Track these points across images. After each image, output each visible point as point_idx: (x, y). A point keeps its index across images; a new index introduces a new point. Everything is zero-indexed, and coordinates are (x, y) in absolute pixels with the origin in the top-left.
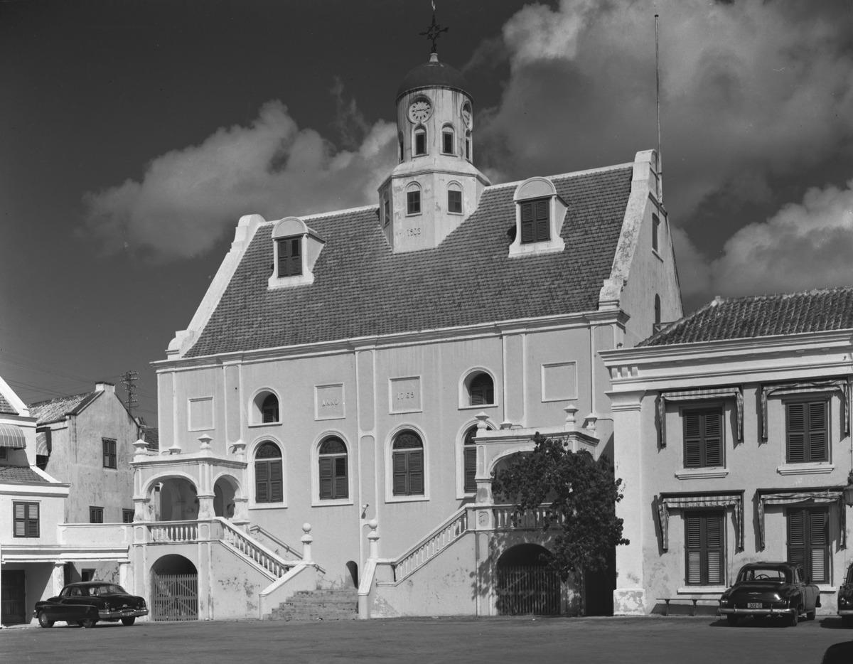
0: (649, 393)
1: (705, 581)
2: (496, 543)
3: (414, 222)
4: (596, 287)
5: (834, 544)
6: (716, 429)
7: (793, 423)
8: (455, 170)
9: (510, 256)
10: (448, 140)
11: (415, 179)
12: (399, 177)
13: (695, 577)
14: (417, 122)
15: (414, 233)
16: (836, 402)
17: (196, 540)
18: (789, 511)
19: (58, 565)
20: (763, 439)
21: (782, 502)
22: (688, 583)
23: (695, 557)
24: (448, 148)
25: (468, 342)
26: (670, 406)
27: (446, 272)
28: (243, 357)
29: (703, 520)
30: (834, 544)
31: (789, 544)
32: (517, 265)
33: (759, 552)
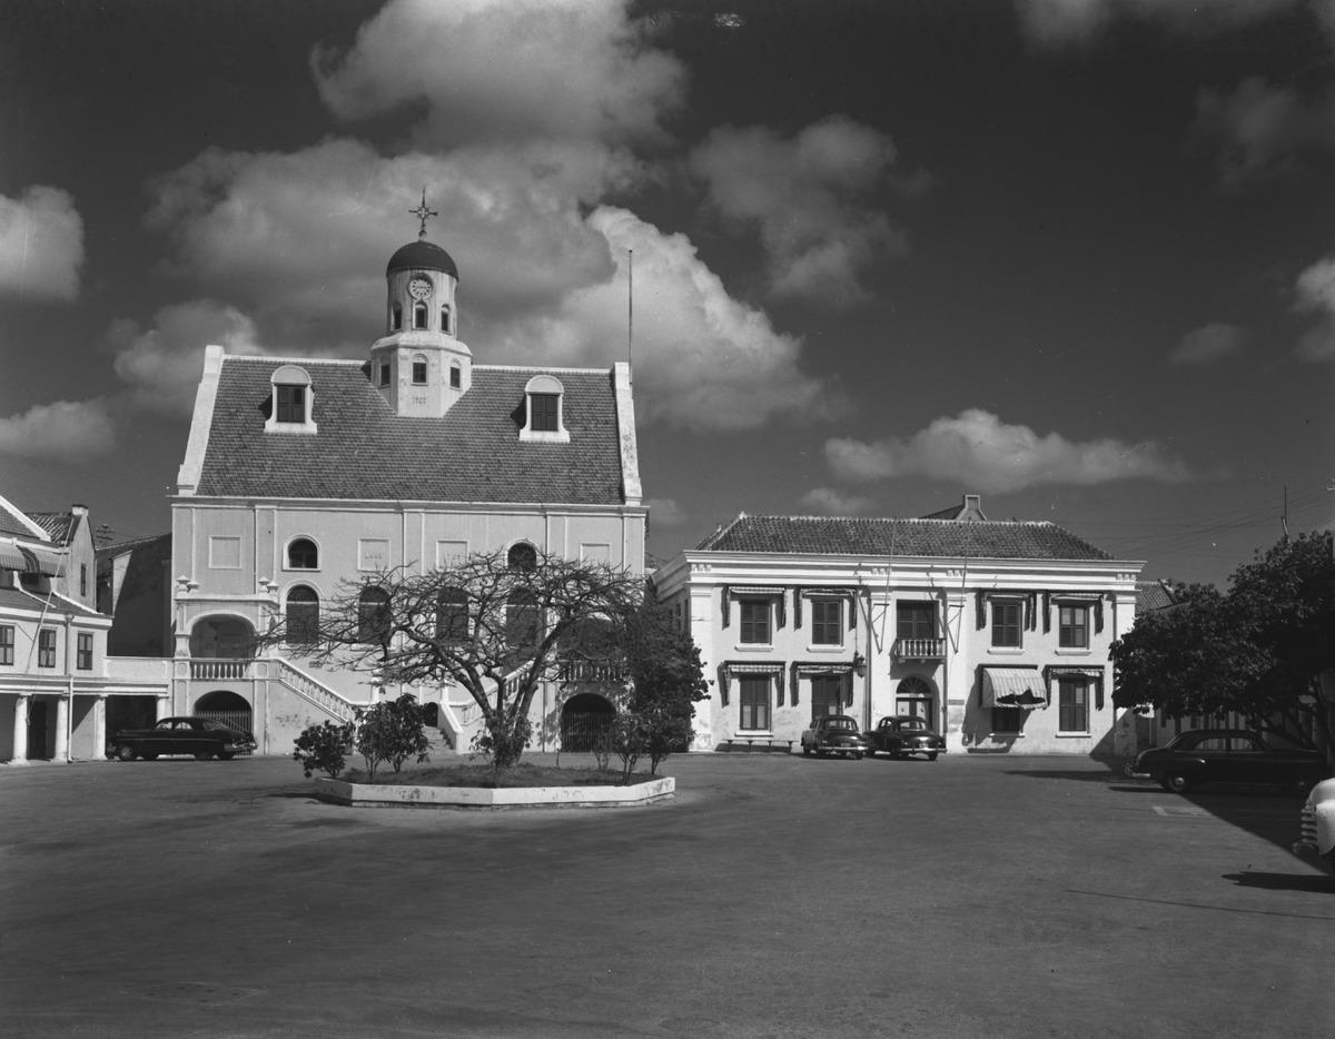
0: (718, 585)
1: (754, 727)
2: (561, 698)
3: (419, 391)
5: (844, 704)
6: (765, 616)
7: (817, 616)
8: (455, 349)
10: (445, 317)
11: (422, 352)
12: (406, 347)
13: (747, 723)
14: (419, 298)
15: (420, 401)
16: (846, 603)
18: (814, 678)
19: (102, 699)
20: (798, 624)
21: (812, 672)
22: (742, 728)
23: (747, 709)
24: (445, 327)
25: (515, 517)
26: (735, 596)
27: (461, 444)
28: (280, 503)
29: (754, 683)
30: (844, 704)
31: (813, 701)
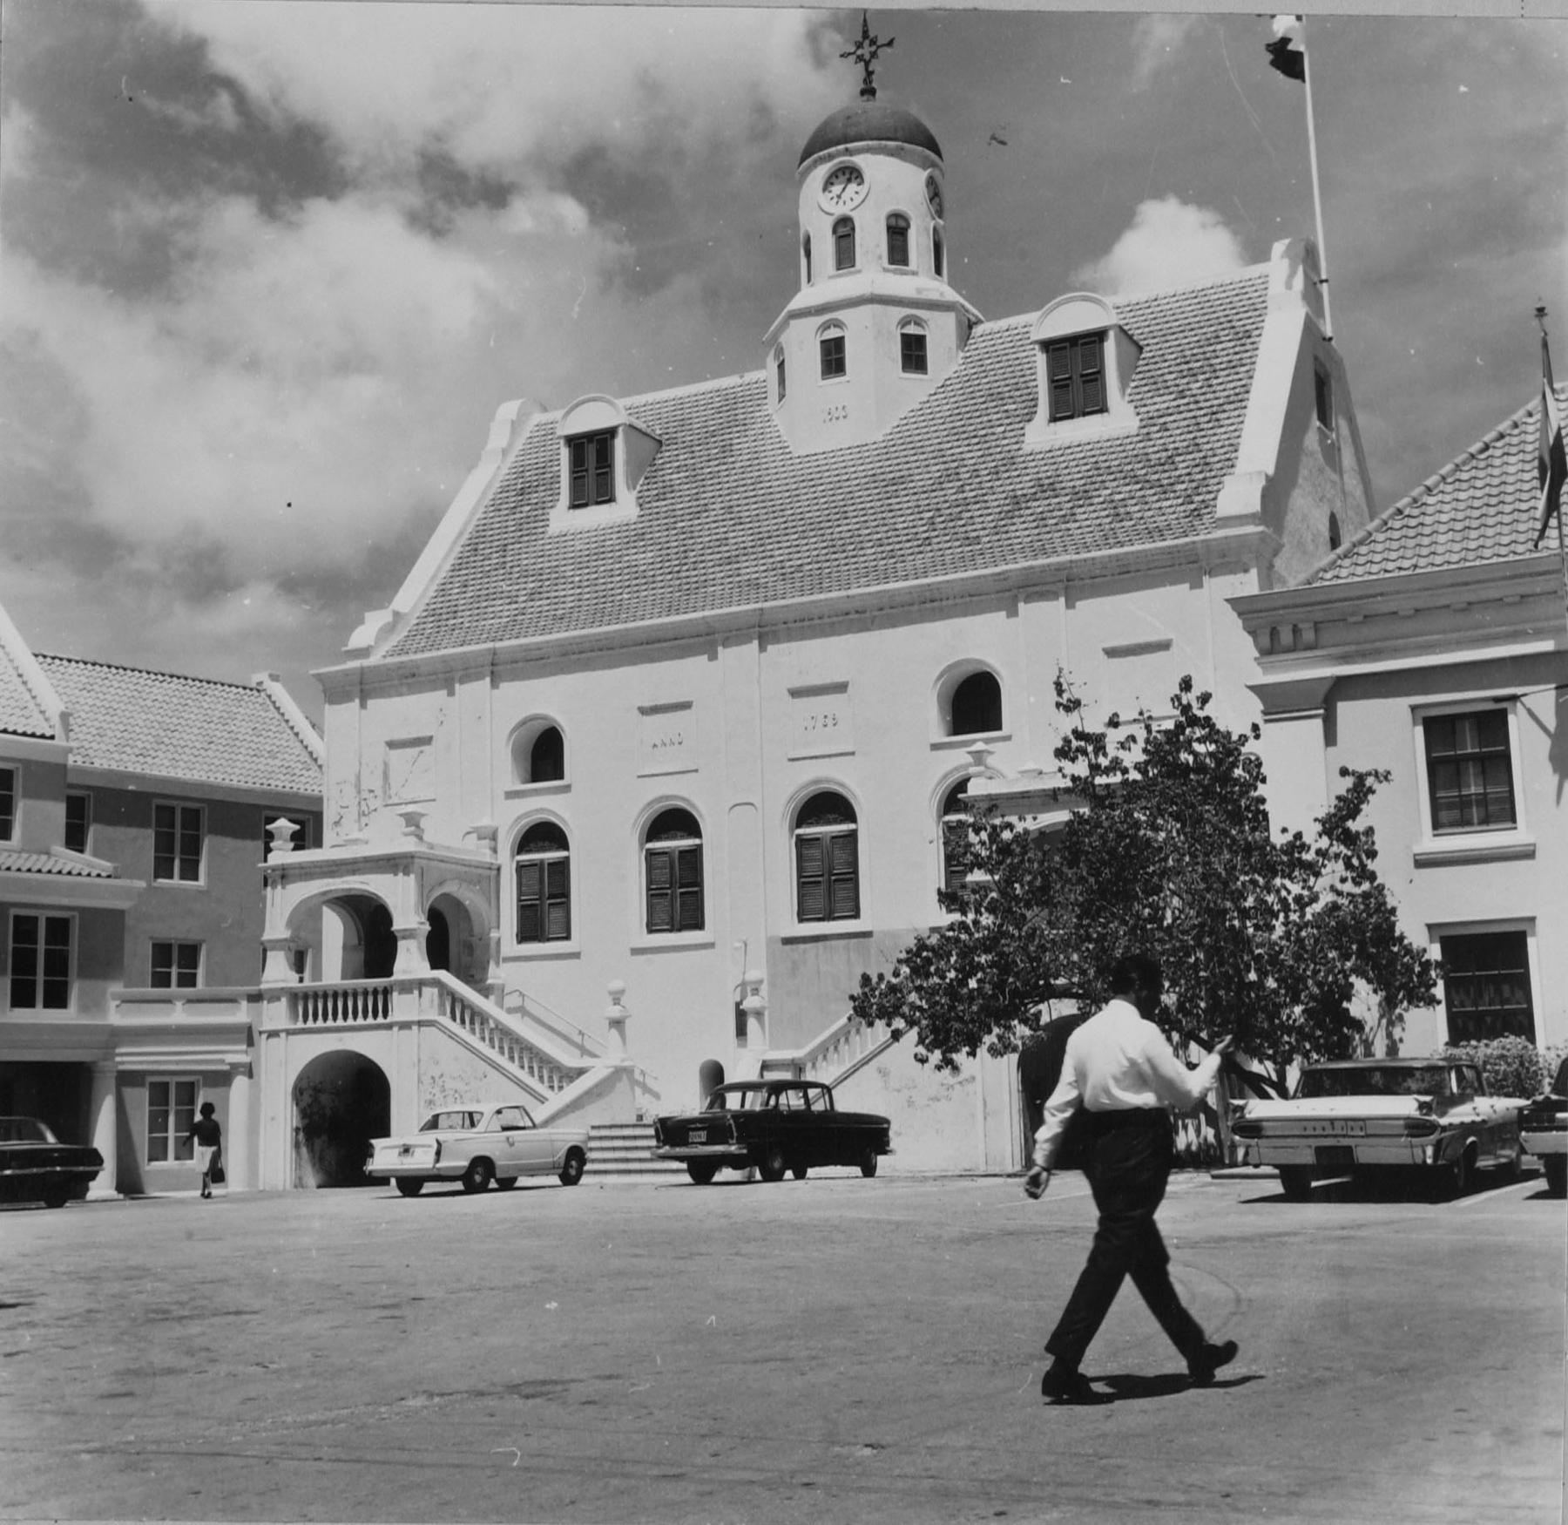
4: (1210, 492)
9: (1027, 448)
17: (389, 1020)
24: (898, 253)
32: (1043, 462)
33: (1270, 57)
